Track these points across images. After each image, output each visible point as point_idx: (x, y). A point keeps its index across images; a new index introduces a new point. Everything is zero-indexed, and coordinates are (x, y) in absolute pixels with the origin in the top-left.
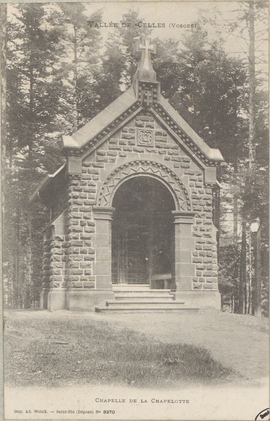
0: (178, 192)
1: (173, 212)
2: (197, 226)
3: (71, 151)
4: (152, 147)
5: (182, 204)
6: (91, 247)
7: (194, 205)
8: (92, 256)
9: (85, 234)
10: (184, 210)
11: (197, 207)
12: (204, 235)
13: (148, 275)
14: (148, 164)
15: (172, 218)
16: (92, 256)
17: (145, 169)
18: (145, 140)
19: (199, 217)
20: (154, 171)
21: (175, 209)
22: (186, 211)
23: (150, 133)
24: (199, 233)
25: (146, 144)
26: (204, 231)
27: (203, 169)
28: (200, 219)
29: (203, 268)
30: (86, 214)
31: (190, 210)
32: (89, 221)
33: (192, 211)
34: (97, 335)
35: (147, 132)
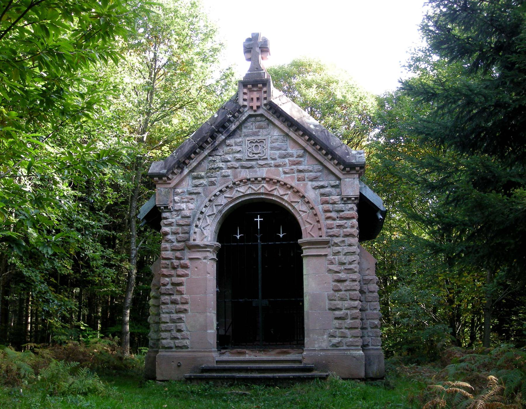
0: (305, 214)
1: (299, 241)
2: (334, 258)
3: (155, 178)
4: (266, 159)
5: (310, 230)
6: (184, 296)
7: (329, 228)
8: (185, 307)
9: (176, 280)
10: (313, 237)
11: (331, 232)
12: (346, 269)
13: (178, 396)
14: (231, 188)
15: (298, 249)
16: (185, 307)
17: (256, 189)
18: (256, 152)
19: (336, 244)
20: (270, 189)
21: (301, 238)
22: (316, 238)
23: (263, 142)
24: (334, 267)
25: (256, 156)
26: (344, 264)
27: (339, 179)
28: (338, 248)
29: (343, 316)
30: (178, 254)
31: (321, 236)
32: (182, 262)
33: (325, 238)
34: (453, 184)
35: (259, 141)
